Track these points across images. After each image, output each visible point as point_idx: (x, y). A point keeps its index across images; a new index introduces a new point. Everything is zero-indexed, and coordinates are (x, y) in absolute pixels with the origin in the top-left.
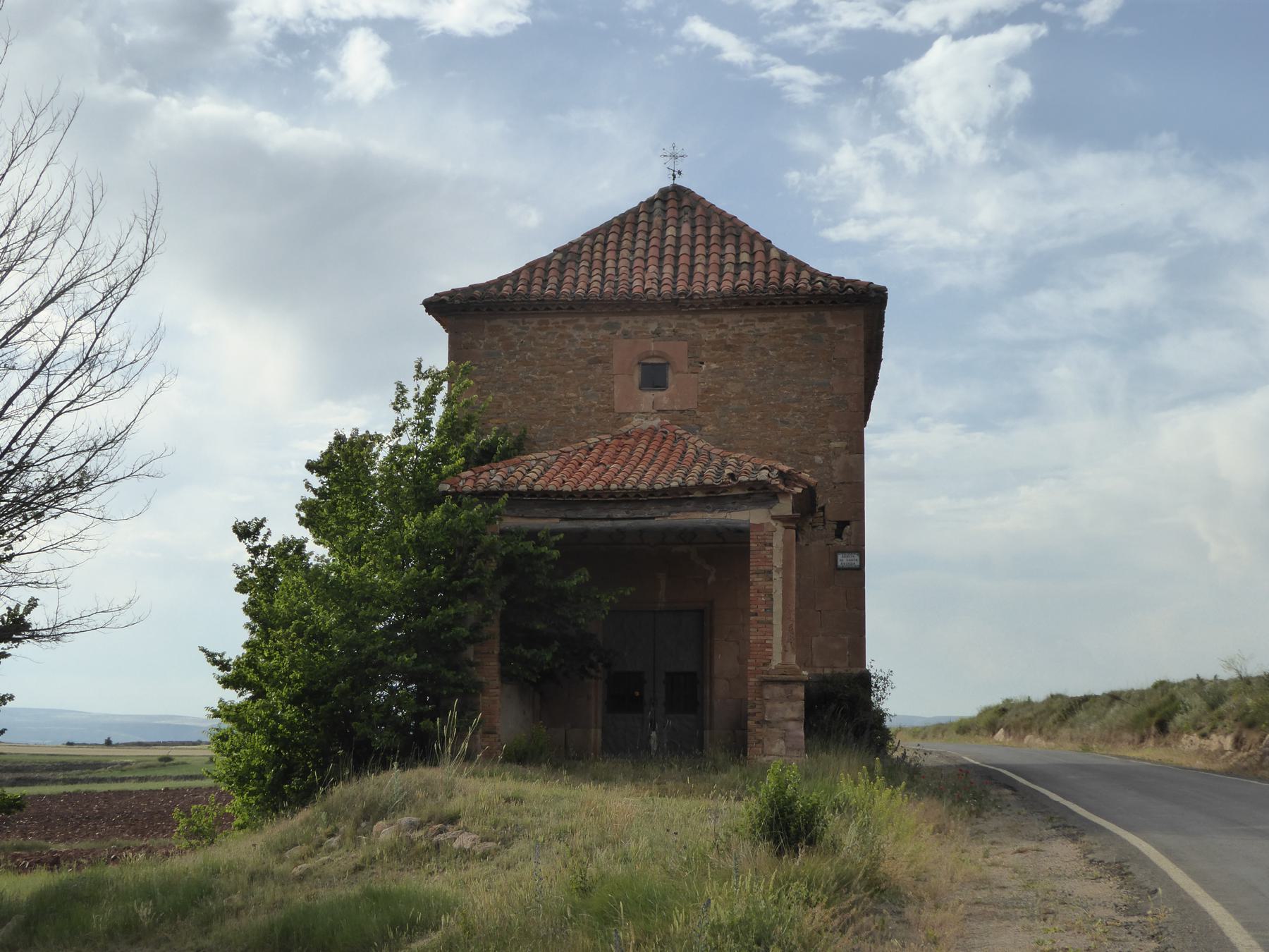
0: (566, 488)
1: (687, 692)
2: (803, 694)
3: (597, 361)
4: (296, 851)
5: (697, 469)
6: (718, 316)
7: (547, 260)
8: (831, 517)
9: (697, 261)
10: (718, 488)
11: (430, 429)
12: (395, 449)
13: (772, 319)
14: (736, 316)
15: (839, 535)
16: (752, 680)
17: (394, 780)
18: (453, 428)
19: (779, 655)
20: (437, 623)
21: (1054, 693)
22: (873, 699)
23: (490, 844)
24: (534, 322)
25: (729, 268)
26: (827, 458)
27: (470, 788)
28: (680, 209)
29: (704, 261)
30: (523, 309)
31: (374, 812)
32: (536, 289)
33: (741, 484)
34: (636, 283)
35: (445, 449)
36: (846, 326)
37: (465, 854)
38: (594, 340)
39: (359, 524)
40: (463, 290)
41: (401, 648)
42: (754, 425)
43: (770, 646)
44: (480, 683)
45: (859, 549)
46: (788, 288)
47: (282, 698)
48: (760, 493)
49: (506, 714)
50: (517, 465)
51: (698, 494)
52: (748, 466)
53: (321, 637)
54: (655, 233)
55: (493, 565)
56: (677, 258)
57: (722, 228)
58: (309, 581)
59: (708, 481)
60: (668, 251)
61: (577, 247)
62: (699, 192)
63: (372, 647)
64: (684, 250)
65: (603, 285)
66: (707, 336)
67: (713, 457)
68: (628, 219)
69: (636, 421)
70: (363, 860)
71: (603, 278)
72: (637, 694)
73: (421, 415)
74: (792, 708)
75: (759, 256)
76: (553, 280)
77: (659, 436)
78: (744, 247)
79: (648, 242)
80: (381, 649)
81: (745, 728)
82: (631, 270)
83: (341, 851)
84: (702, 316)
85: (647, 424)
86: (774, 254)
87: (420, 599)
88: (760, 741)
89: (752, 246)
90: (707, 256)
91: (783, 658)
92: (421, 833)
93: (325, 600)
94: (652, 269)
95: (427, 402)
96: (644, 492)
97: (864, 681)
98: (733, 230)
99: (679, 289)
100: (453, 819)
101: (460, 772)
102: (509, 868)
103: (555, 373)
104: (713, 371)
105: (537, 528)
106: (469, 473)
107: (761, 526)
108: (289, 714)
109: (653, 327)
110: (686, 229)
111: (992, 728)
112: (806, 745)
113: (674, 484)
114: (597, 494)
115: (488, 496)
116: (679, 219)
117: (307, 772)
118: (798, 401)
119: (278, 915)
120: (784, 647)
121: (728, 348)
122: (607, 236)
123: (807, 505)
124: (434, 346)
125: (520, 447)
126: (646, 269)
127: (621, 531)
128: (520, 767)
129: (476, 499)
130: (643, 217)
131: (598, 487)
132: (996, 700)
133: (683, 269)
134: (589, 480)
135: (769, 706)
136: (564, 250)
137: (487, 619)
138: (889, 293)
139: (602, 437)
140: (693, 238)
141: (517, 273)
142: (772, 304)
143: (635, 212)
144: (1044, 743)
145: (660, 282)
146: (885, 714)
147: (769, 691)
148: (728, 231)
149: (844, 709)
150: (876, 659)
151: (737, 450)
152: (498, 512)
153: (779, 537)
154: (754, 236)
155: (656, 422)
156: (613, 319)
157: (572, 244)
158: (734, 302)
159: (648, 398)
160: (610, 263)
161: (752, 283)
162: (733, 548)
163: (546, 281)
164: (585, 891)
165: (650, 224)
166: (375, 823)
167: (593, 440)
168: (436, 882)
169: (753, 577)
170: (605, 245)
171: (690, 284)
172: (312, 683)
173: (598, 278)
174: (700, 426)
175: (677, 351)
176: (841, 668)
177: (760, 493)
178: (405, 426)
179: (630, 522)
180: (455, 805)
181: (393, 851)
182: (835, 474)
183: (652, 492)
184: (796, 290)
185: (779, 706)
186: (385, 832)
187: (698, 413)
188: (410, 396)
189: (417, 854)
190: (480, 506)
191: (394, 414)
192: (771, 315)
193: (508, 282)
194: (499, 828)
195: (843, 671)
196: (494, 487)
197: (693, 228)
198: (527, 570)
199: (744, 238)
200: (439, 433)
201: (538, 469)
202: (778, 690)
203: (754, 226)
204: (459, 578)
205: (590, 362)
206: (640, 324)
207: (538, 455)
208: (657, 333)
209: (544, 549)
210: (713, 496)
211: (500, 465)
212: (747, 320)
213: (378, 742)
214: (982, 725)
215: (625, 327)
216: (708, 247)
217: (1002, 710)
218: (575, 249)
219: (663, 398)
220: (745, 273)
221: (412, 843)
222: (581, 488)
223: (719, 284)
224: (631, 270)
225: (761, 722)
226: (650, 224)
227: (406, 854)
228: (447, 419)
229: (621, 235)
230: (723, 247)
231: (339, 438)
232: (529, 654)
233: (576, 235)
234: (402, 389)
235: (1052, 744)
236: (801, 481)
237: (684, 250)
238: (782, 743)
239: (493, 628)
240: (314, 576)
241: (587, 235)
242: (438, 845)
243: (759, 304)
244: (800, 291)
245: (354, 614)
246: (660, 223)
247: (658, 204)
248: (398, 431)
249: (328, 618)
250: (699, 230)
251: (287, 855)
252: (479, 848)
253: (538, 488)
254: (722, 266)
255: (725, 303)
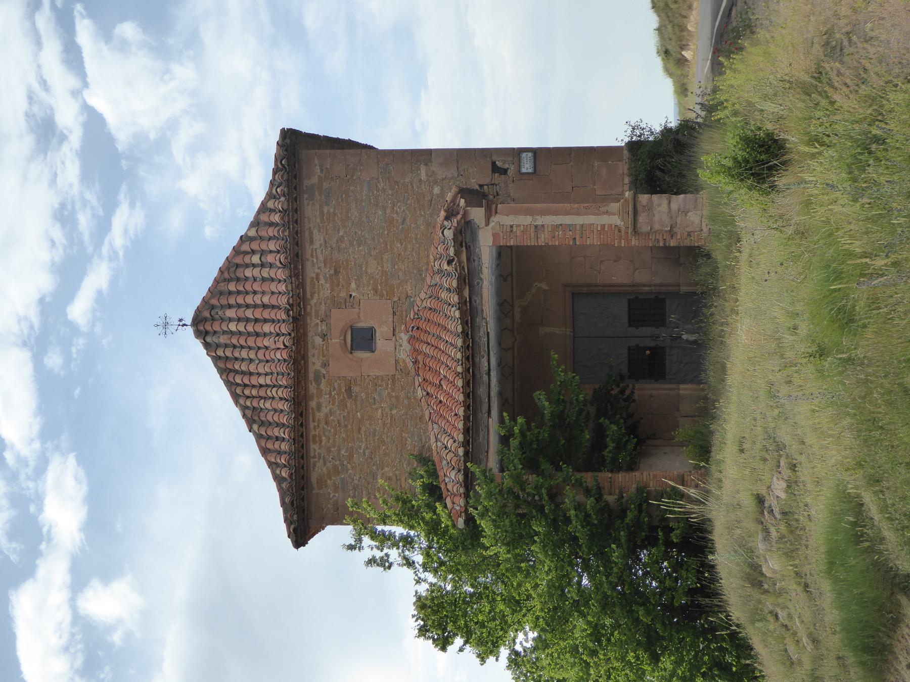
0: (461, 412)
1: (647, 308)
2: (646, 196)
3: (349, 390)
4: (792, 648)
5: (443, 295)
6: (308, 282)
7: (259, 437)
8: (489, 175)
9: (259, 302)
10: (460, 274)
11: (408, 536)
12: (425, 567)
13: (311, 233)
14: (308, 265)
15: (504, 172)
16: (634, 242)
17: (725, 560)
18: (409, 515)
19: (611, 218)
20: (583, 527)
21: (650, 5)
22: (651, 139)
23: (782, 464)
24: (314, 448)
25: (265, 273)
26: (436, 182)
27: (729, 495)
28: (213, 319)
29: (259, 296)
30: (302, 457)
31: (755, 577)
32: (284, 446)
33: (457, 253)
34: (278, 356)
35: (427, 523)
36: (315, 170)
37: (791, 485)
38: (330, 394)
39: (494, 600)
40: (285, 512)
41: (606, 560)
42: (406, 249)
43: (603, 226)
44: (638, 489)
45: (517, 153)
46: (282, 218)
47: (653, 671)
48: (465, 237)
49: (663, 469)
50: (441, 459)
51: (466, 293)
52: (440, 248)
53: (597, 634)
54: (234, 341)
55: (532, 478)
56: (256, 320)
57: (229, 280)
58: (547, 646)
59: (455, 284)
60: (250, 328)
61: (247, 411)
62: (198, 302)
63: (605, 585)
64: (249, 313)
65: (280, 386)
66: (326, 291)
67: (433, 282)
68: (222, 365)
69: (402, 355)
70: (799, 584)
71: (274, 386)
72: (648, 352)
73: (395, 545)
74: (659, 205)
75: (255, 246)
76: (276, 432)
77: (416, 333)
78: (247, 260)
79: (242, 347)
80: (607, 577)
81: (677, 249)
82: (267, 361)
83: (791, 606)
84: (308, 296)
85: (406, 346)
86: (252, 233)
87: (562, 543)
88: (689, 235)
89: (246, 253)
90: (255, 293)
91: (614, 214)
92: (773, 530)
93: (564, 632)
94: (266, 343)
95: (384, 539)
96: (464, 342)
97: (634, 146)
98: (231, 271)
99: (284, 317)
100: (760, 500)
101: (718, 498)
102: (803, 443)
103: (360, 429)
104: (358, 286)
105: (497, 438)
106: (448, 501)
107: (495, 236)
108: (667, 662)
109: (318, 340)
110: (231, 313)
111: (682, 62)
112: (692, 193)
113: (457, 314)
114: (467, 384)
115: (468, 481)
116: (222, 320)
117: (721, 649)
118: (384, 209)
119: (851, 659)
120: (604, 213)
121: (337, 272)
122: (238, 385)
123: (475, 196)
124: (332, 538)
125: (425, 460)
126: (267, 348)
127: (500, 364)
128: (713, 449)
129: (471, 493)
130: (220, 352)
131: (460, 383)
132: (657, 63)
133: (266, 314)
134: (454, 393)
135: (657, 227)
136: (250, 422)
137: (579, 483)
138: (287, 127)
139: (417, 384)
140: (239, 306)
141: (270, 464)
142: (297, 233)
143: (216, 359)
144: (694, 12)
145: (278, 335)
146: (665, 128)
147: (644, 227)
148: (232, 275)
149: (659, 162)
150: (614, 136)
151: (428, 263)
152: (484, 472)
153: (504, 219)
154: (236, 251)
155: (404, 337)
156: (311, 376)
157: (244, 416)
158: (296, 268)
159: (381, 343)
160: (261, 381)
161: (278, 252)
162: (515, 262)
163: (277, 438)
164: (822, 353)
165: (226, 346)
166: (762, 574)
167: (420, 393)
168: (818, 514)
169: (541, 242)
170: (245, 385)
171: (279, 308)
172: (639, 644)
173: (274, 390)
174: (407, 297)
175: (340, 319)
176: (623, 167)
177: (465, 237)
178: (406, 558)
179: (491, 353)
180: (748, 502)
181: (790, 554)
182: (449, 175)
183: (465, 334)
184: (284, 212)
185: (657, 218)
186: (773, 565)
187: (396, 299)
188: (378, 554)
189: (792, 532)
190: (477, 487)
191: (395, 567)
192: (307, 235)
193: (278, 472)
194: (768, 457)
195: (626, 167)
196: (461, 477)
197: (230, 306)
198: (535, 446)
199: (238, 260)
200: (412, 527)
201: (445, 439)
202: (642, 219)
203: (228, 251)
204: (543, 507)
205: (350, 397)
206: (316, 352)
207: (433, 440)
208: (324, 336)
209: (516, 430)
210: (468, 279)
211: (441, 474)
212: (312, 256)
213: (691, 582)
214: (679, 72)
215: (318, 366)
216: (247, 293)
217: (666, 53)
218: (249, 413)
219: (382, 331)
220: (270, 258)
221: (782, 537)
222: (461, 398)
223: (280, 281)
224: (267, 361)
225: (672, 233)
226: (226, 346)
227: (792, 542)
228: (400, 522)
229: (236, 372)
230: (246, 279)
231: (423, 631)
232: (611, 446)
233: (236, 412)
234: (371, 562)
235: (695, 5)
236: (453, 200)
237: (249, 313)
238: (690, 214)
239: (588, 478)
240: (541, 644)
241: (236, 403)
242: (784, 513)
243: (297, 244)
244: (285, 207)
245: (576, 604)
246: (226, 337)
247: (208, 339)
248: (409, 563)
249: (579, 627)
250: (232, 301)
251: (794, 657)
252: (786, 473)
253: (461, 438)
254: (264, 280)
255: (297, 275)
